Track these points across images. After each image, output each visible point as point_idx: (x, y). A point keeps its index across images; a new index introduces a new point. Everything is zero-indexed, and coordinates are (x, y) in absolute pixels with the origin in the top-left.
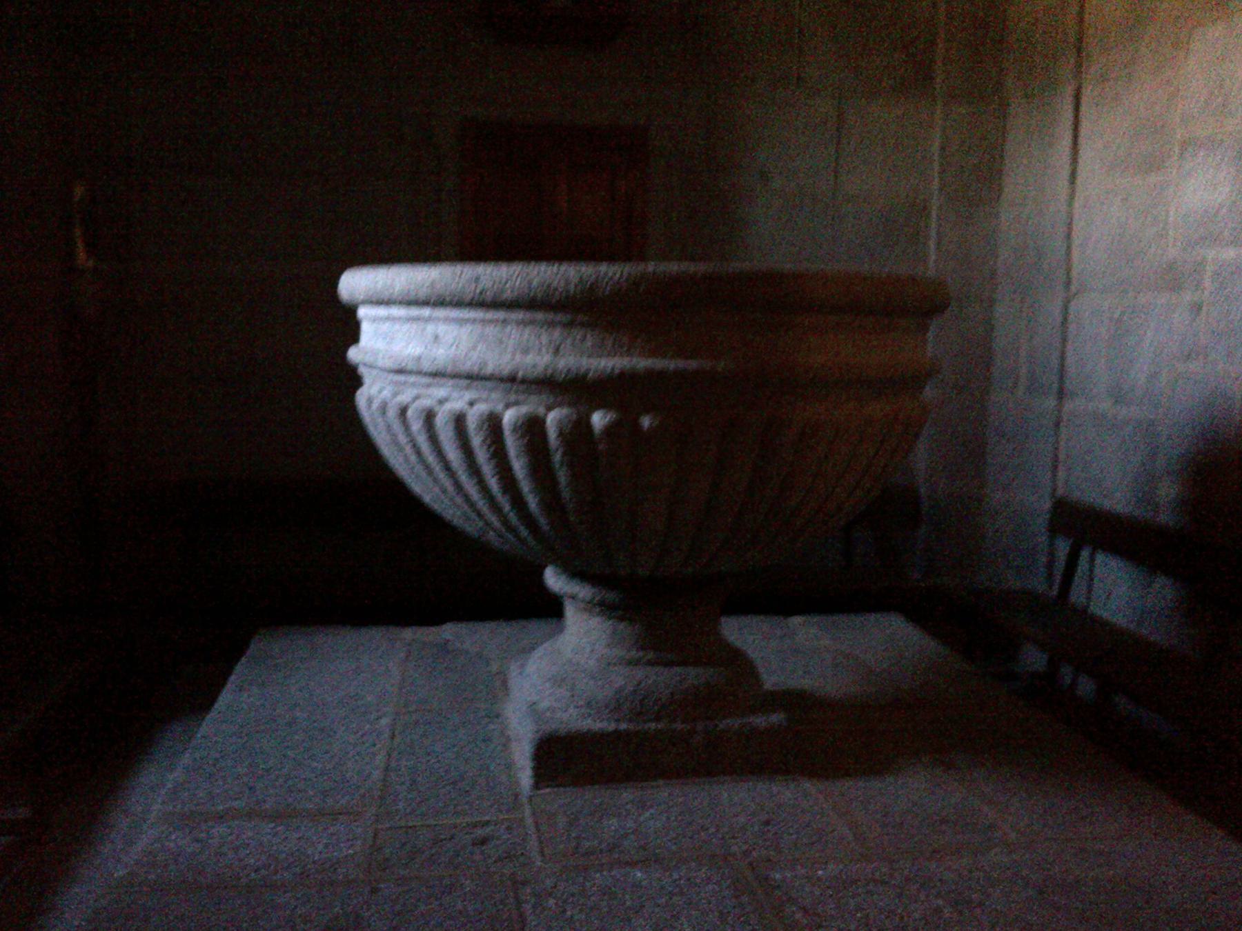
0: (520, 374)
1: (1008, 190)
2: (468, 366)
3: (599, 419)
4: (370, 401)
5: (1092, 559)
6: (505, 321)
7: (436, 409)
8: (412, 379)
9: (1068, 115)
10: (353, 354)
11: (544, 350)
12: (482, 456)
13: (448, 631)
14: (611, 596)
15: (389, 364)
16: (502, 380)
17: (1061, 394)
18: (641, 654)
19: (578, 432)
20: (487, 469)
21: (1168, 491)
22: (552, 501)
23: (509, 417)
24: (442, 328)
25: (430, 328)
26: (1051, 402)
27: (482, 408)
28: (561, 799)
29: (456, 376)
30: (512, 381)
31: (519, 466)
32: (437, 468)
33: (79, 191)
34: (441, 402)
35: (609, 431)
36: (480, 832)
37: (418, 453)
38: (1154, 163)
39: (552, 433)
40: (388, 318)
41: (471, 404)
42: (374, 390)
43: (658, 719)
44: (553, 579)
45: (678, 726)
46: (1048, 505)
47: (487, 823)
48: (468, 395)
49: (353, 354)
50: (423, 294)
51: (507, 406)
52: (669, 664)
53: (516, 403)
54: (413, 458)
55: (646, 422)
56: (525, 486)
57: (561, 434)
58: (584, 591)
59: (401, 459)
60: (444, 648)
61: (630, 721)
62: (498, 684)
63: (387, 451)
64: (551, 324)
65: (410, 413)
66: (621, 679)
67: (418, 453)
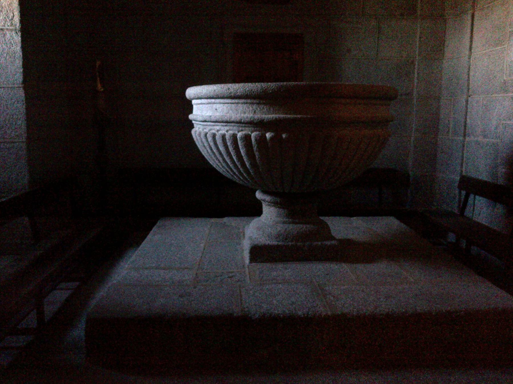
0: (243, 121)
1: (447, 55)
2: (225, 119)
3: (268, 135)
4: (196, 131)
5: (475, 198)
6: (238, 103)
7: (217, 133)
8: (209, 123)
9: (469, 23)
10: (191, 117)
11: (251, 112)
12: (231, 149)
13: (225, 220)
14: (278, 200)
15: (201, 119)
16: (237, 123)
17: (465, 135)
18: (287, 220)
19: (261, 140)
20: (233, 153)
21: (502, 170)
22: (254, 165)
23: (239, 135)
24: (218, 106)
25: (214, 105)
26: (461, 138)
27: (231, 132)
28: (258, 267)
29: (222, 122)
30: (239, 122)
31: (243, 151)
32: (217, 154)
33: (98, 63)
34: (218, 131)
35: (272, 138)
36: (231, 275)
37: (211, 149)
38: (499, 42)
39: (253, 139)
40: (201, 104)
41: (227, 131)
42: (197, 129)
43: (292, 241)
44: (259, 195)
45: (299, 244)
46: (458, 178)
47: (233, 272)
48: (227, 128)
49: (191, 117)
50: (212, 94)
51: (238, 132)
52: (296, 223)
53: (242, 130)
54: (209, 151)
55: (284, 136)
56: (245, 158)
57: (256, 140)
58: (268, 198)
59: (206, 152)
60: (224, 225)
61: (282, 242)
62: (241, 235)
63: (204, 153)
64: (253, 104)
65: (208, 135)
66: (280, 228)
67: (211, 149)
